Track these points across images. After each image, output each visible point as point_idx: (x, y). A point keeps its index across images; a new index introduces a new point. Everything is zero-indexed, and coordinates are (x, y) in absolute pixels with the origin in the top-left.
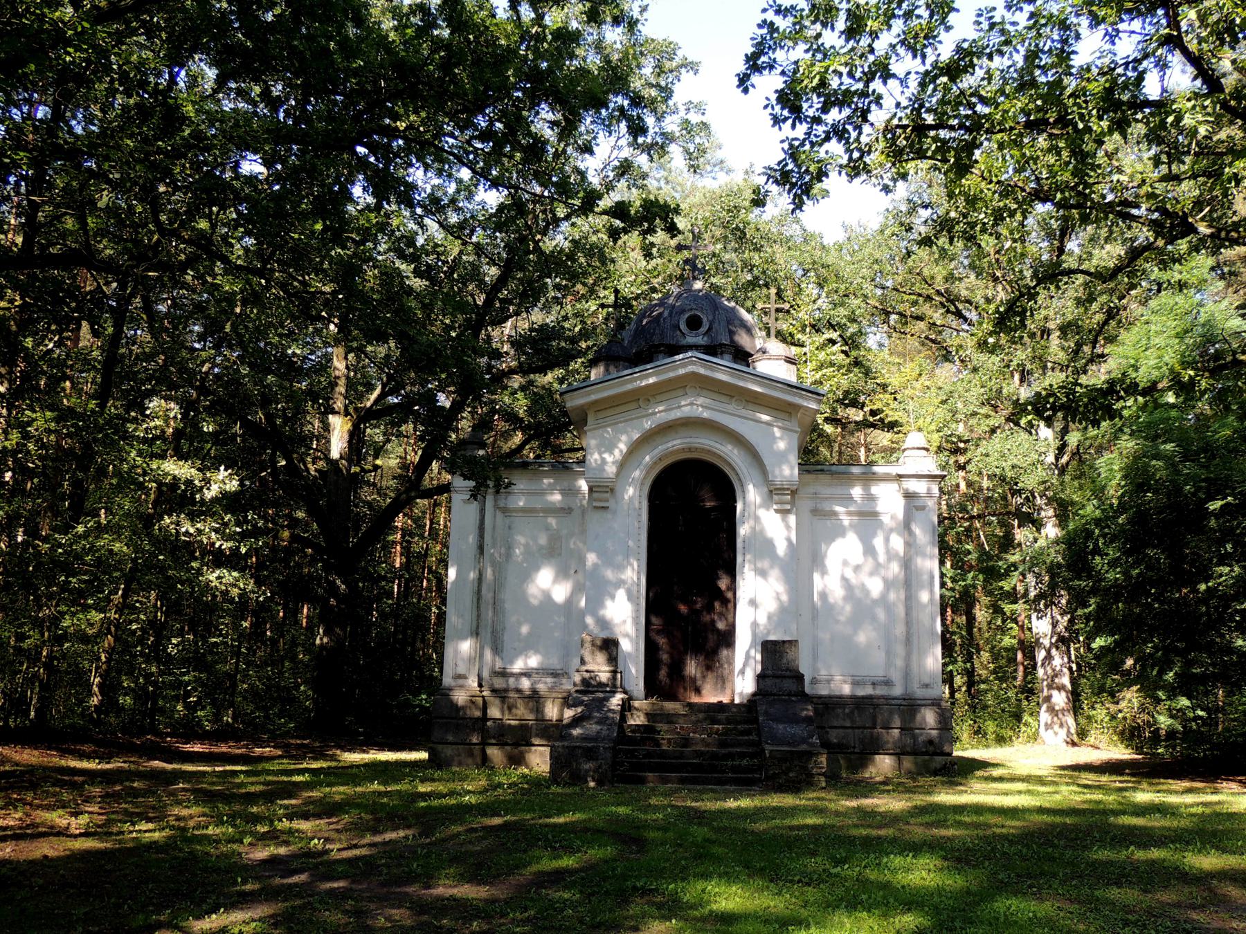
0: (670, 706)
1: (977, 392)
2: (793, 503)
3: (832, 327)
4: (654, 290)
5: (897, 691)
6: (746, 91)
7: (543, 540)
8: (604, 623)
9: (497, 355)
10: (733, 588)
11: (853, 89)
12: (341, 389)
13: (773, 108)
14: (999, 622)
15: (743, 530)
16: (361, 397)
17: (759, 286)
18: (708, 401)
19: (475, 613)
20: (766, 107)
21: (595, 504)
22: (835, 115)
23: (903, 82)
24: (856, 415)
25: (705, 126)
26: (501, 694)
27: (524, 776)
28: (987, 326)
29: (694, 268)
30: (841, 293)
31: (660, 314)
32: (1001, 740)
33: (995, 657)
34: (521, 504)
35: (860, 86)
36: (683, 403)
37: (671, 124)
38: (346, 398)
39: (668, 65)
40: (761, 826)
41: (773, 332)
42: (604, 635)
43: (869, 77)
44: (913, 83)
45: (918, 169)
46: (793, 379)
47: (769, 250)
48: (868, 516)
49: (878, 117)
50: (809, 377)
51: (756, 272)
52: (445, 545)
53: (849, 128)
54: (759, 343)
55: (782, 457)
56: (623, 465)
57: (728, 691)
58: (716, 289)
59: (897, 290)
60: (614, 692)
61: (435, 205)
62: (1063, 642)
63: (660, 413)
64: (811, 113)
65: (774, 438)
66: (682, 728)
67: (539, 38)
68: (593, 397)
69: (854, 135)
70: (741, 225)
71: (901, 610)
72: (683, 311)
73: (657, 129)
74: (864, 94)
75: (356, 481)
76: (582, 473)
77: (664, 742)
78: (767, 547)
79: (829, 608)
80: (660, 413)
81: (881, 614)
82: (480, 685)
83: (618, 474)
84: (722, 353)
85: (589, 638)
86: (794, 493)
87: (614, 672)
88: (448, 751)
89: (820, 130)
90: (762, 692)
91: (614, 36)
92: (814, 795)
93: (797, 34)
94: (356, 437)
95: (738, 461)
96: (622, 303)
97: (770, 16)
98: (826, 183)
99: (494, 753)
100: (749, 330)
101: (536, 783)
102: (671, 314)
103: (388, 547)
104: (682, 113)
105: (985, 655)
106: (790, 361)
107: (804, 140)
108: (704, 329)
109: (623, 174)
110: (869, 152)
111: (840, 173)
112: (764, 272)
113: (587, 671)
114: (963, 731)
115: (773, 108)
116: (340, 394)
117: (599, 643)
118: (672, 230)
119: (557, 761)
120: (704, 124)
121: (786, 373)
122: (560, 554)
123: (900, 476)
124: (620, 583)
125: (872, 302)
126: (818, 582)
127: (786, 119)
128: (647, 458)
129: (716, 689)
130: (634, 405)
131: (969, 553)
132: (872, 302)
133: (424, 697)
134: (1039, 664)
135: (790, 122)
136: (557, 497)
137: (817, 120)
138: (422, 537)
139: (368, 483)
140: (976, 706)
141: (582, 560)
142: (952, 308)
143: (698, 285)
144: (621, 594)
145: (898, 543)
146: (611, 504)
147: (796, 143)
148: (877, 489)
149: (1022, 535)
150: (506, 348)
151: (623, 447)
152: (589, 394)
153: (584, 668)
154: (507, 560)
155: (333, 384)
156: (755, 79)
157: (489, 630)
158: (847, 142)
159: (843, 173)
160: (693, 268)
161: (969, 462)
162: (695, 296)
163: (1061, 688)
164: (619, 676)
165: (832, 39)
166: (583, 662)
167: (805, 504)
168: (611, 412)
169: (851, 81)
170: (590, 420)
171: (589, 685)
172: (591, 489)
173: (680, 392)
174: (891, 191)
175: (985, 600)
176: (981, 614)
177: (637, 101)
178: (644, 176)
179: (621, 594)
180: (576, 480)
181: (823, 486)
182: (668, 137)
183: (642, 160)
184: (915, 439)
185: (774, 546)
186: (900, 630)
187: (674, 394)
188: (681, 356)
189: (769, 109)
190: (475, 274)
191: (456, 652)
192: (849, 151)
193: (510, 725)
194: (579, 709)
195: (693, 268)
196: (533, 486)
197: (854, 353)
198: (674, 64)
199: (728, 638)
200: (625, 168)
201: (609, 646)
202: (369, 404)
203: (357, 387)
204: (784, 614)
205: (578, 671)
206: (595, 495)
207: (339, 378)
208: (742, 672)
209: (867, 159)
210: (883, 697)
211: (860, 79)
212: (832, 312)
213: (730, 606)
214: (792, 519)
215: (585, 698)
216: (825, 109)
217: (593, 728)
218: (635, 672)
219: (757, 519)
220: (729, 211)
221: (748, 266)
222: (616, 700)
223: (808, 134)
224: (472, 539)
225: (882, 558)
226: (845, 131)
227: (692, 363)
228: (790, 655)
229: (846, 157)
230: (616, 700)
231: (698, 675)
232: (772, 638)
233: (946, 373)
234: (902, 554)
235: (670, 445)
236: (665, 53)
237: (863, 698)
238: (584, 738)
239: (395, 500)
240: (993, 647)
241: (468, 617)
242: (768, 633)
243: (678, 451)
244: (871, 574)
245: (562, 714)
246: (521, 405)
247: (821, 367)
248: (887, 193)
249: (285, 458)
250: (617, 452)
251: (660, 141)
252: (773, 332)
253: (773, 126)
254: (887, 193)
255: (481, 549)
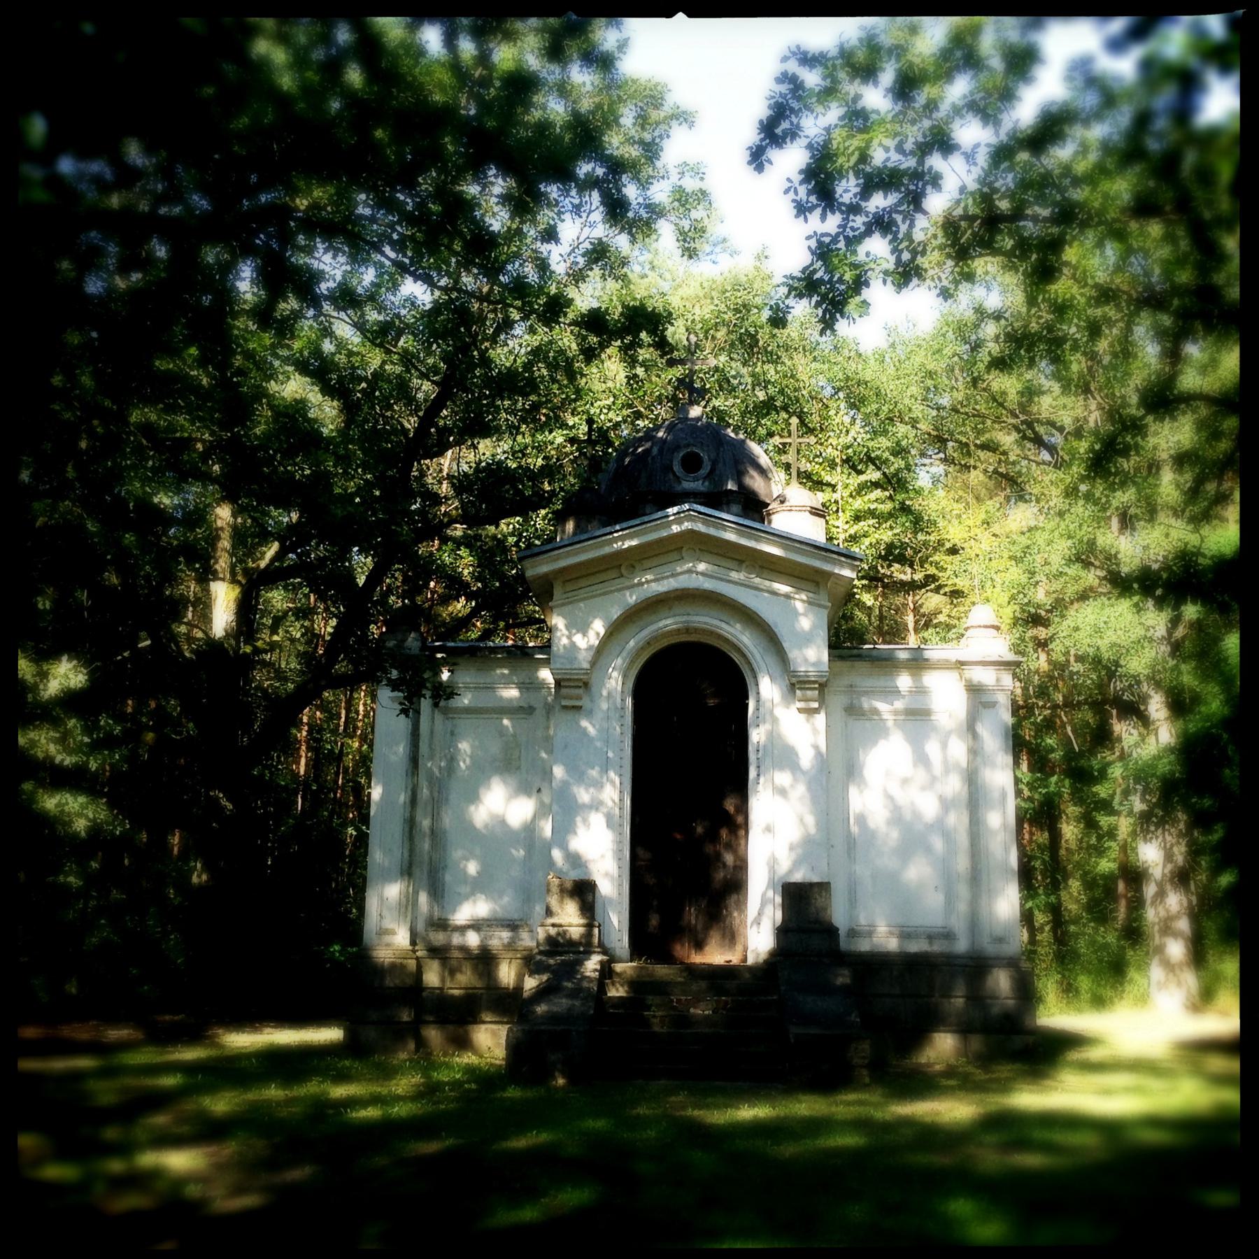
0: (662, 971)
1: (1063, 547)
2: (822, 699)
3: (870, 460)
4: (638, 415)
5: (961, 946)
6: (760, 168)
7: (495, 748)
8: (575, 860)
9: (435, 499)
10: (743, 808)
11: (903, 167)
12: (225, 543)
13: (796, 193)
14: (1093, 841)
15: (756, 736)
16: (251, 552)
17: (775, 408)
18: (710, 567)
19: (407, 845)
20: (787, 192)
21: (564, 703)
22: (879, 202)
23: (970, 157)
24: (901, 573)
25: (703, 195)
26: (438, 952)
27: (470, 1070)
28: (1077, 469)
29: (691, 390)
30: (882, 416)
31: (647, 452)
32: (1099, 1002)
33: (1090, 883)
34: (466, 702)
35: (910, 163)
36: (679, 569)
37: (660, 193)
38: (231, 555)
39: (654, 115)
40: (789, 1150)
41: (794, 472)
42: (574, 875)
43: (924, 149)
44: (982, 159)
45: (985, 265)
46: (821, 539)
47: (789, 363)
48: (918, 715)
49: (937, 203)
50: (842, 526)
51: (771, 390)
52: (367, 739)
53: (899, 218)
54: (776, 490)
55: (807, 639)
56: (600, 652)
57: (739, 948)
58: (720, 414)
59: (957, 411)
60: (588, 953)
61: (347, 298)
62: (1181, 878)
63: (651, 584)
64: (846, 198)
65: (796, 613)
66: (679, 1001)
67: (485, 82)
68: (563, 563)
69: (903, 228)
70: (752, 330)
71: (963, 839)
72: (677, 448)
73: (641, 200)
74: (917, 175)
75: (247, 664)
76: (547, 662)
77: (655, 1021)
78: (787, 758)
79: (870, 835)
80: (651, 584)
81: (938, 844)
82: (413, 943)
83: (594, 663)
84: (728, 503)
85: (556, 881)
86: (822, 687)
87: (590, 926)
88: (371, 1033)
89: (859, 221)
90: (781, 955)
91: (581, 77)
92: (852, 1097)
93: (829, 92)
94: (246, 609)
95: (752, 648)
96: (599, 436)
97: (793, 67)
98: (866, 293)
99: (433, 1035)
100: (763, 472)
101: (486, 1080)
102: (661, 451)
103: (290, 749)
104: (674, 178)
105: (1075, 885)
106: (816, 512)
107: (838, 235)
108: (704, 471)
109: (596, 261)
110: (923, 253)
111: (885, 282)
112: (782, 392)
113: (553, 925)
114: (1049, 987)
115: (796, 193)
116: (224, 550)
117: (569, 885)
118: (662, 345)
119: (515, 1049)
120: (703, 193)
121: (813, 531)
122: (518, 768)
123: (962, 663)
124: (596, 805)
125: (923, 426)
126: (854, 794)
127: (813, 208)
128: (632, 643)
129: (722, 946)
130: (613, 574)
131: (1052, 750)
132: (923, 426)
133: (337, 948)
134: (1149, 901)
135: (819, 211)
136: (512, 693)
137: (854, 209)
138: (335, 732)
139: (265, 664)
140: (1065, 957)
141: (548, 774)
142: (1029, 433)
143: (695, 412)
144: (597, 820)
145: (959, 750)
146: (585, 702)
147: (827, 240)
148: (931, 679)
149: (1125, 731)
150: (445, 488)
151: (598, 627)
152: (558, 558)
153: (550, 921)
154: (449, 775)
155: (213, 539)
156: (773, 154)
157: (426, 868)
158: (895, 239)
159: (889, 279)
160: (690, 389)
161: (1052, 639)
162: (694, 429)
163: (1176, 935)
164: (596, 931)
165: (876, 98)
166: (549, 912)
167: (837, 701)
168: (583, 583)
169: (900, 157)
170: (558, 592)
171: (557, 944)
172: (558, 683)
173: (675, 556)
174: (951, 296)
175: (1072, 810)
176: (1070, 831)
177: (617, 167)
178: (624, 262)
179: (597, 820)
180: (537, 670)
181: (860, 676)
182: (656, 211)
183: (621, 242)
184: (981, 614)
185: (797, 755)
186: (962, 863)
187: (662, 559)
188: (675, 509)
189: (792, 194)
190: (403, 391)
191: (382, 900)
192: (896, 251)
193: (452, 996)
194: (545, 977)
195: (690, 389)
196: (482, 679)
197: (900, 497)
198: (662, 114)
199: (736, 884)
200: (599, 254)
201: (583, 891)
202: (263, 564)
203: (246, 541)
204: (808, 848)
205: (543, 925)
206: (564, 691)
207: (222, 529)
208: (757, 922)
209: (919, 260)
210: (942, 955)
211: (912, 153)
212: (871, 444)
213: (742, 832)
214: (820, 719)
215: (551, 962)
216: (866, 193)
217: (561, 1004)
218: (617, 921)
219: (775, 720)
220: (737, 311)
221: (759, 381)
222: (592, 964)
223: (843, 227)
224: (401, 750)
225: (938, 768)
226: (892, 223)
227: (690, 518)
228: (820, 901)
229: (892, 259)
230: (592, 964)
231: (699, 927)
232: (798, 877)
233: (1021, 516)
234: (964, 764)
235: (661, 624)
236: (651, 98)
237: (916, 955)
238: (552, 1018)
239: (299, 688)
240: (1086, 874)
241: (397, 853)
242: (790, 872)
243: (671, 633)
244: (923, 788)
245: (520, 979)
246: (465, 563)
247: (857, 518)
248: (946, 299)
249: (151, 637)
250: (591, 634)
251: (645, 216)
252: (794, 472)
253: (797, 216)
254: (946, 299)
255: (414, 760)
